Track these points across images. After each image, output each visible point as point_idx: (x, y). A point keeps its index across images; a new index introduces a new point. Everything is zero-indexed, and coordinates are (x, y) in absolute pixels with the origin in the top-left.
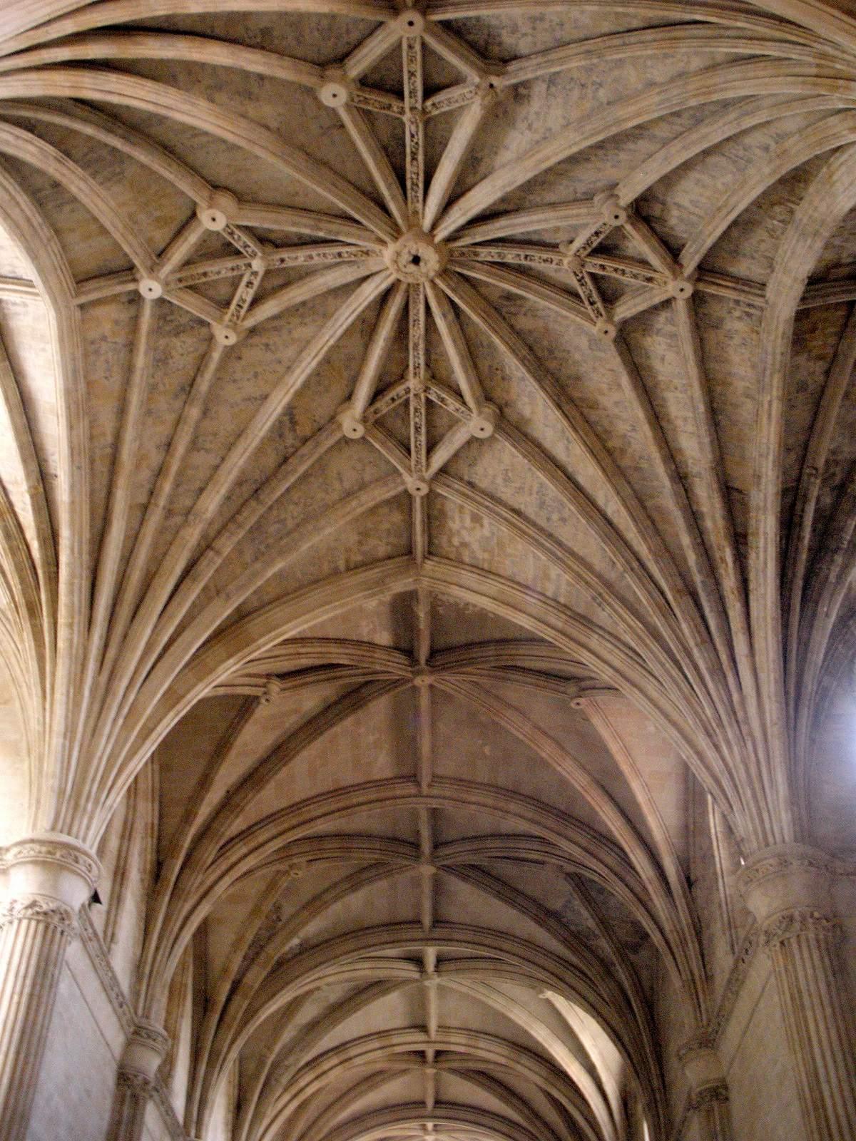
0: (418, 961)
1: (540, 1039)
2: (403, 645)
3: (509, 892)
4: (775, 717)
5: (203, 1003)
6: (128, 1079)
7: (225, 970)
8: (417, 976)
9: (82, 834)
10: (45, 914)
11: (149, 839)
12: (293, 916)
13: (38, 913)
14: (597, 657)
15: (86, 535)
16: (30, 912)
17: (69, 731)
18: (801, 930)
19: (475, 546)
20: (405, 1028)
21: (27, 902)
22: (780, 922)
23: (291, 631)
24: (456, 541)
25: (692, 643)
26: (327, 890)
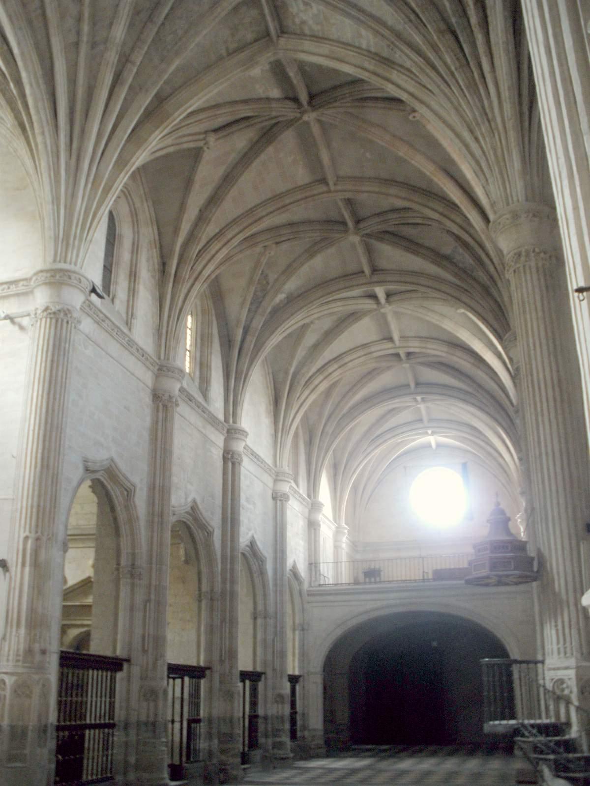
0: (374, 297)
1: (464, 339)
2: (291, 95)
3: (412, 246)
4: (509, 115)
5: (227, 343)
6: (159, 397)
7: (238, 321)
8: (375, 306)
9: (74, 260)
10: (54, 313)
11: (155, 250)
12: (277, 280)
13: (50, 314)
14: (397, 85)
15: (40, 73)
16: (45, 314)
17: (56, 200)
18: (526, 261)
19: (311, 22)
20: (379, 341)
21: (43, 308)
22: (514, 257)
23: (196, 104)
24: (297, 21)
25: (453, 68)
26: (294, 261)
